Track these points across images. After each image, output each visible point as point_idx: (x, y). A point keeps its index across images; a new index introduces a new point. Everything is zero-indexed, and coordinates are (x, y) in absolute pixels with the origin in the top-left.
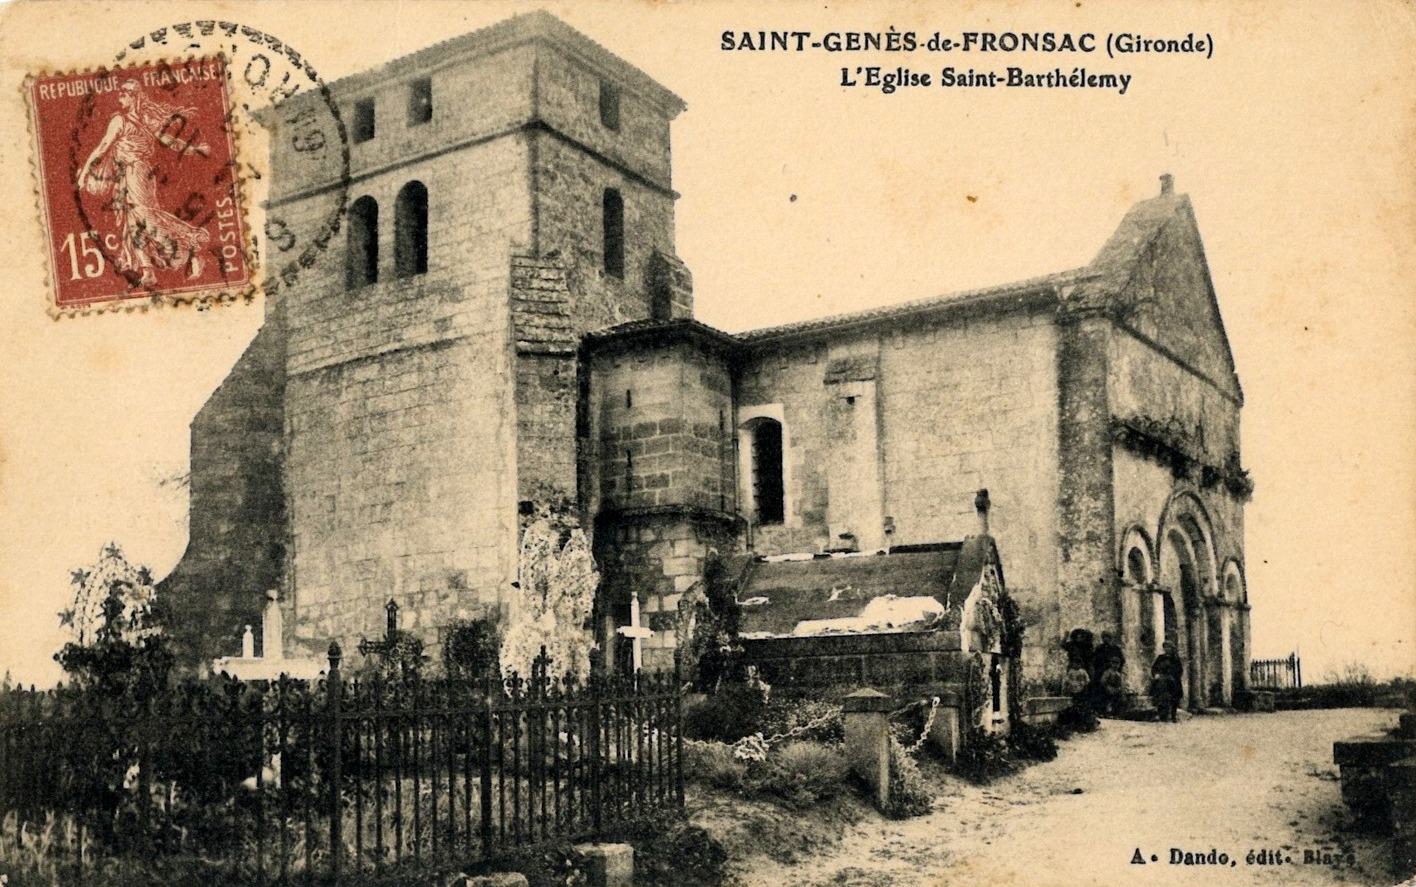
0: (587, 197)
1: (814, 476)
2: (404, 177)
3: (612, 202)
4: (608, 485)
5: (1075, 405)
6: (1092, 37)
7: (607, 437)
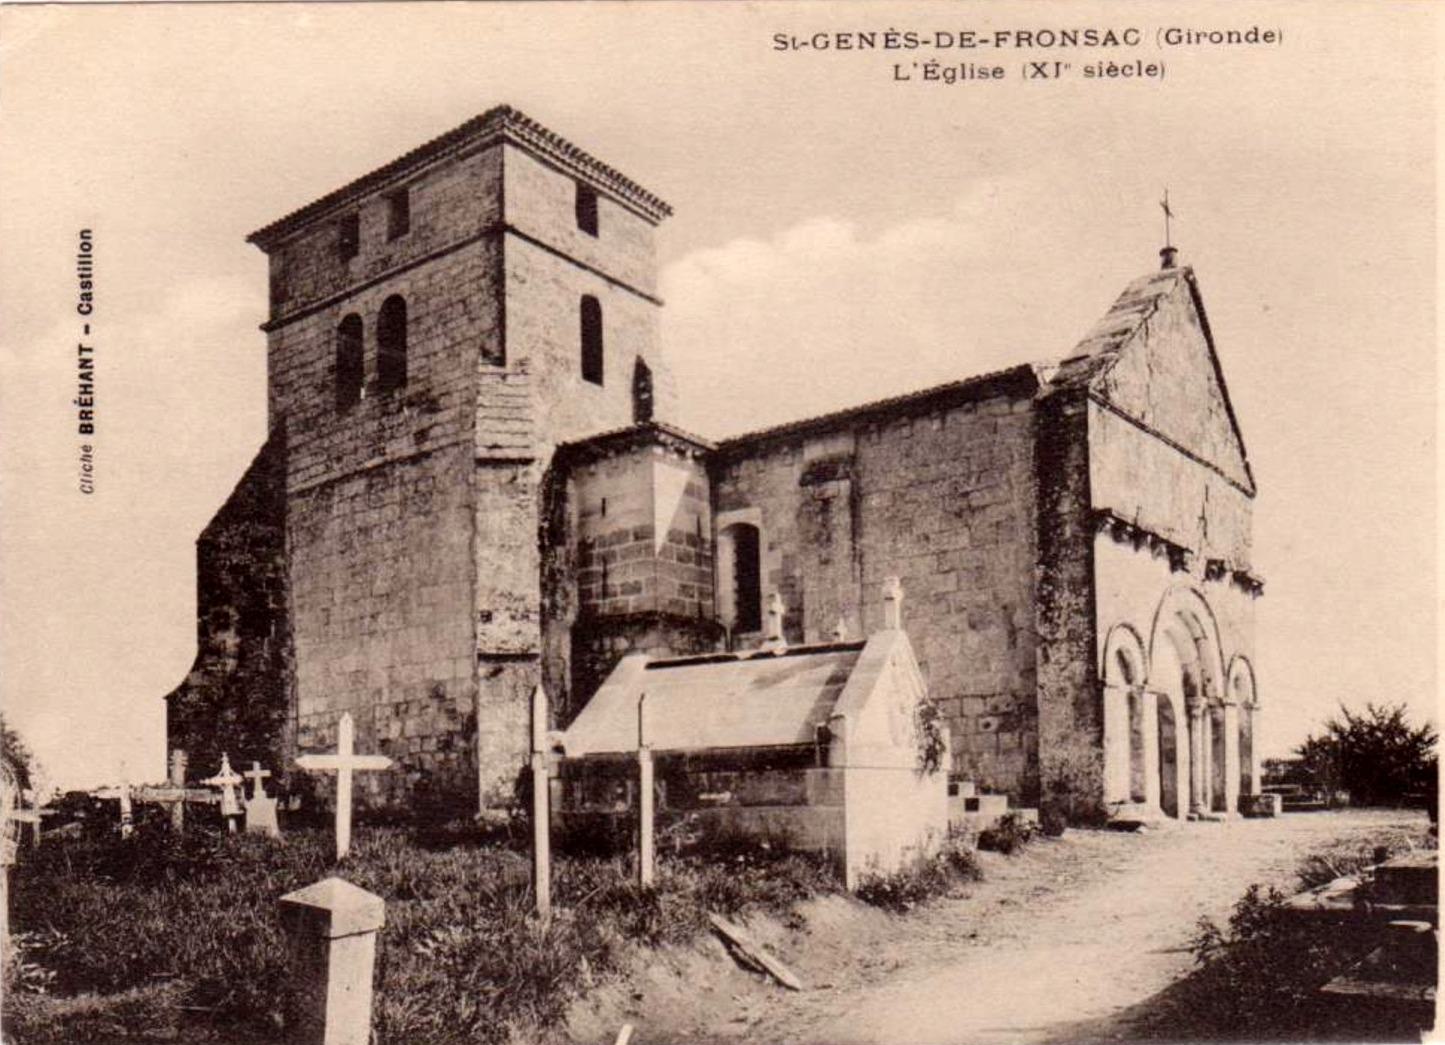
0: (562, 302)
1: (791, 581)
2: (386, 290)
3: (591, 310)
4: (584, 595)
5: (1055, 496)
6: (1136, 31)
7: (585, 547)
